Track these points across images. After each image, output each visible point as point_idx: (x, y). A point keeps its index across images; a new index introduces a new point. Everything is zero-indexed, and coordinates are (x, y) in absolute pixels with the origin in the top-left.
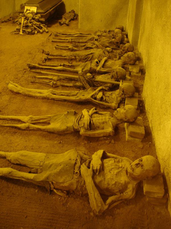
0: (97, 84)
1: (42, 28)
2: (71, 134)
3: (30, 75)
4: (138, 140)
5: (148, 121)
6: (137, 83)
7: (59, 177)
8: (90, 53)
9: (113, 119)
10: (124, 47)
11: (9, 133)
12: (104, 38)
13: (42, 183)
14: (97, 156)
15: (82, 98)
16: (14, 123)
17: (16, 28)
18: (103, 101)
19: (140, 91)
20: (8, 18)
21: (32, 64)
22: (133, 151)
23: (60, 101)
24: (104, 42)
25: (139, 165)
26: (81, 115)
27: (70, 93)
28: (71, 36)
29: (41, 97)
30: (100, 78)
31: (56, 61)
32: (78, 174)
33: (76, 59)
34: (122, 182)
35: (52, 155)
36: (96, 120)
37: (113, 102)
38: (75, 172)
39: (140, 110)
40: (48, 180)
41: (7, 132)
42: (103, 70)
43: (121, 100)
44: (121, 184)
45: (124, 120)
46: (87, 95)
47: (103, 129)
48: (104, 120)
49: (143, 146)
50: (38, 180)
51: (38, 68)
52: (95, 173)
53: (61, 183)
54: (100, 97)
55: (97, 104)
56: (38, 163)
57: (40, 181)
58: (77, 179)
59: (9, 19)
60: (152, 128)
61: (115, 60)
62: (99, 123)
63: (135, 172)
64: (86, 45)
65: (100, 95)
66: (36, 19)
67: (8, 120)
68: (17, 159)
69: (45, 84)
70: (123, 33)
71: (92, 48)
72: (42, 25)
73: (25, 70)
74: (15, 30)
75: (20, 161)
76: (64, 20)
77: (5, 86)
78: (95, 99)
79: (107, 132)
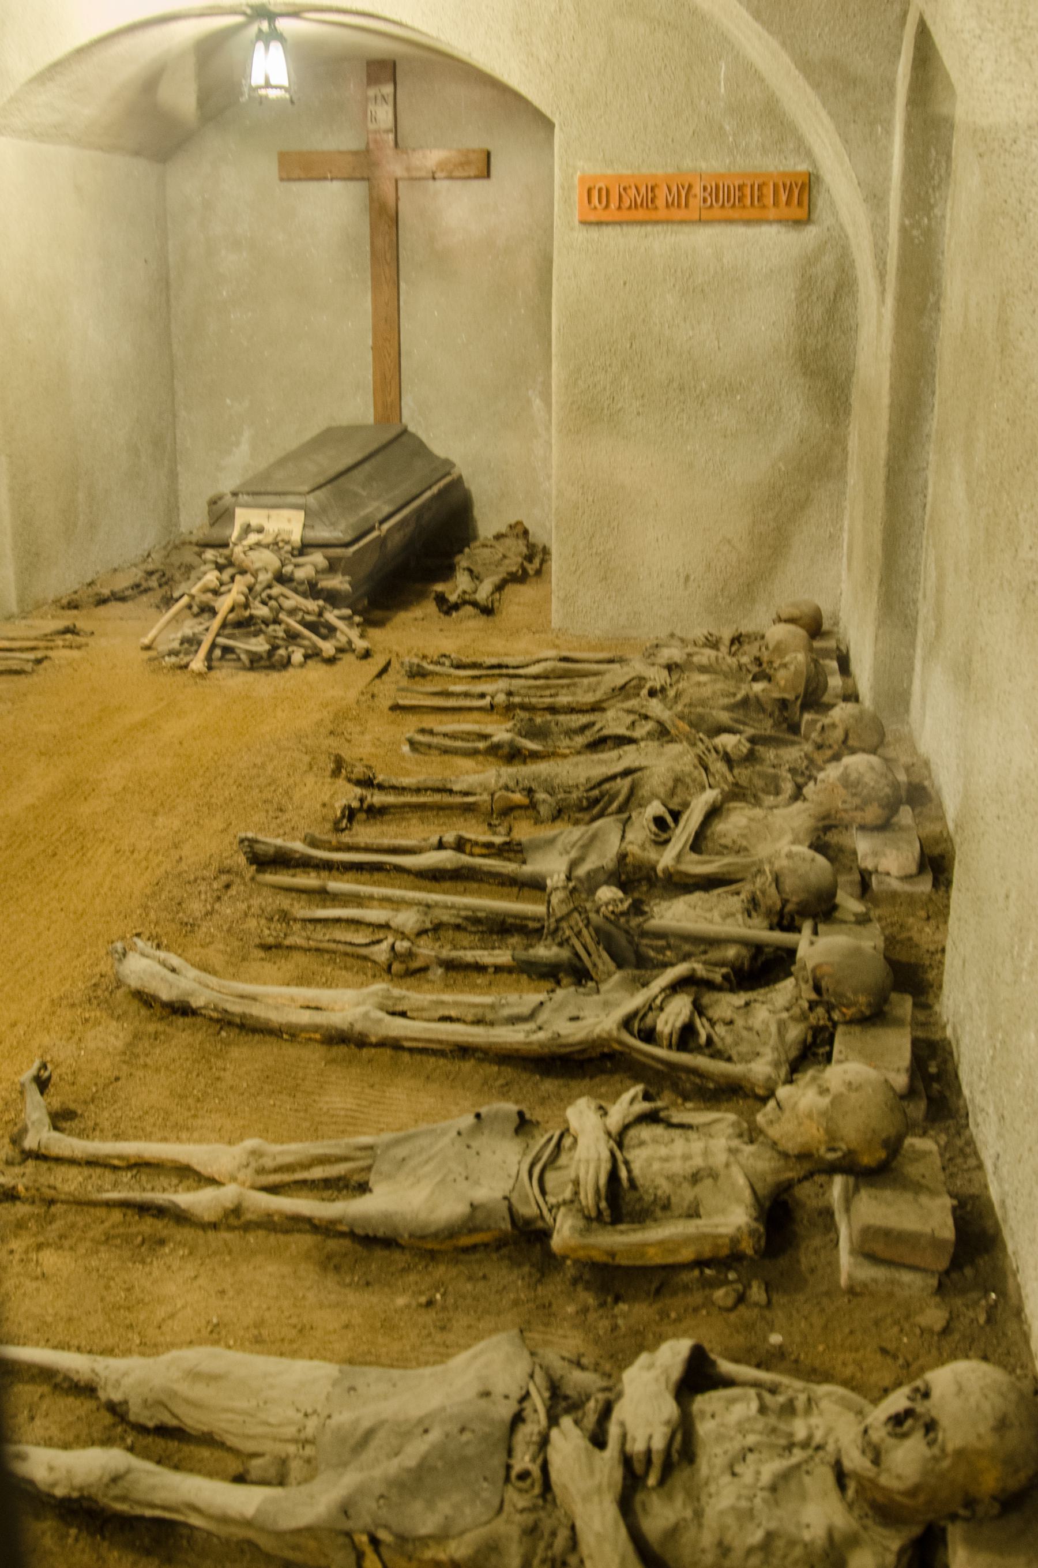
0: (661, 950)
1: (332, 630)
2: (498, 1248)
3: (256, 902)
4: (913, 1283)
5: (980, 1166)
6: (910, 939)
7: (418, 1506)
8: (619, 768)
9: (753, 1154)
10: (823, 727)
11: (118, 1241)
12: (704, 678)
13: (312, 1544)
14: (648, 1376)
15: (567, 1036)
16: (149, 1187)
17: (179, 635)
18: (699, 1050)
19: (932, 986)
20: (136, 575)
21: (268, 840)
22: (884, 1351)
23: (434, 1053)
24: (703, 703)
25: (909, 1423)
26: (562, 1136)
27: (492, 1007)
28: (504, 671)
29: (316, 1028)
30: (675, 914)
31: (414, 821)
32: (533, 1485)
33: (533, 806)
34: (807, 1536)
35: (373, 1372)
36: (649, 1162)
37: (758, 1054)
38: (514, 1473)
39: (930, 1100)
40: (349, 1525)
41: (108, 1239)
42: (697, 866)
43: (809, 1039)
44: (806, 1545)
45: (821, 1159)
46: (596, 1015)
47: (693, 1213)
48: (698, 1162)
49: (947, 1315)
50: (287, 1523)
51: (305, 864)
52: (633, 1480)
53: (424, 1541)
54: (679, 1024)
55: (660, 1067)
56: (291, 1423)
57: (298, 1532)
58: (525, 1516)
59: (138, 586)
60: (1003, 1203)
61: (771, 808)
62: (669, 1178)
63: (888, 1470)
64: (593, 724)
65: (677, 1011)
66: (302, 583)
67: (115, 1168)
68: (164, 1398)
69: (346, 954)
70: (817, 644)
71: (631, 741)
72: (331, 616)
73: (224, 878)
74: (176, 645)
75: (181, 1410)
76: (462, 582)
77: (104, 967)
78: (649, 1036)
79: (720, 1236)
